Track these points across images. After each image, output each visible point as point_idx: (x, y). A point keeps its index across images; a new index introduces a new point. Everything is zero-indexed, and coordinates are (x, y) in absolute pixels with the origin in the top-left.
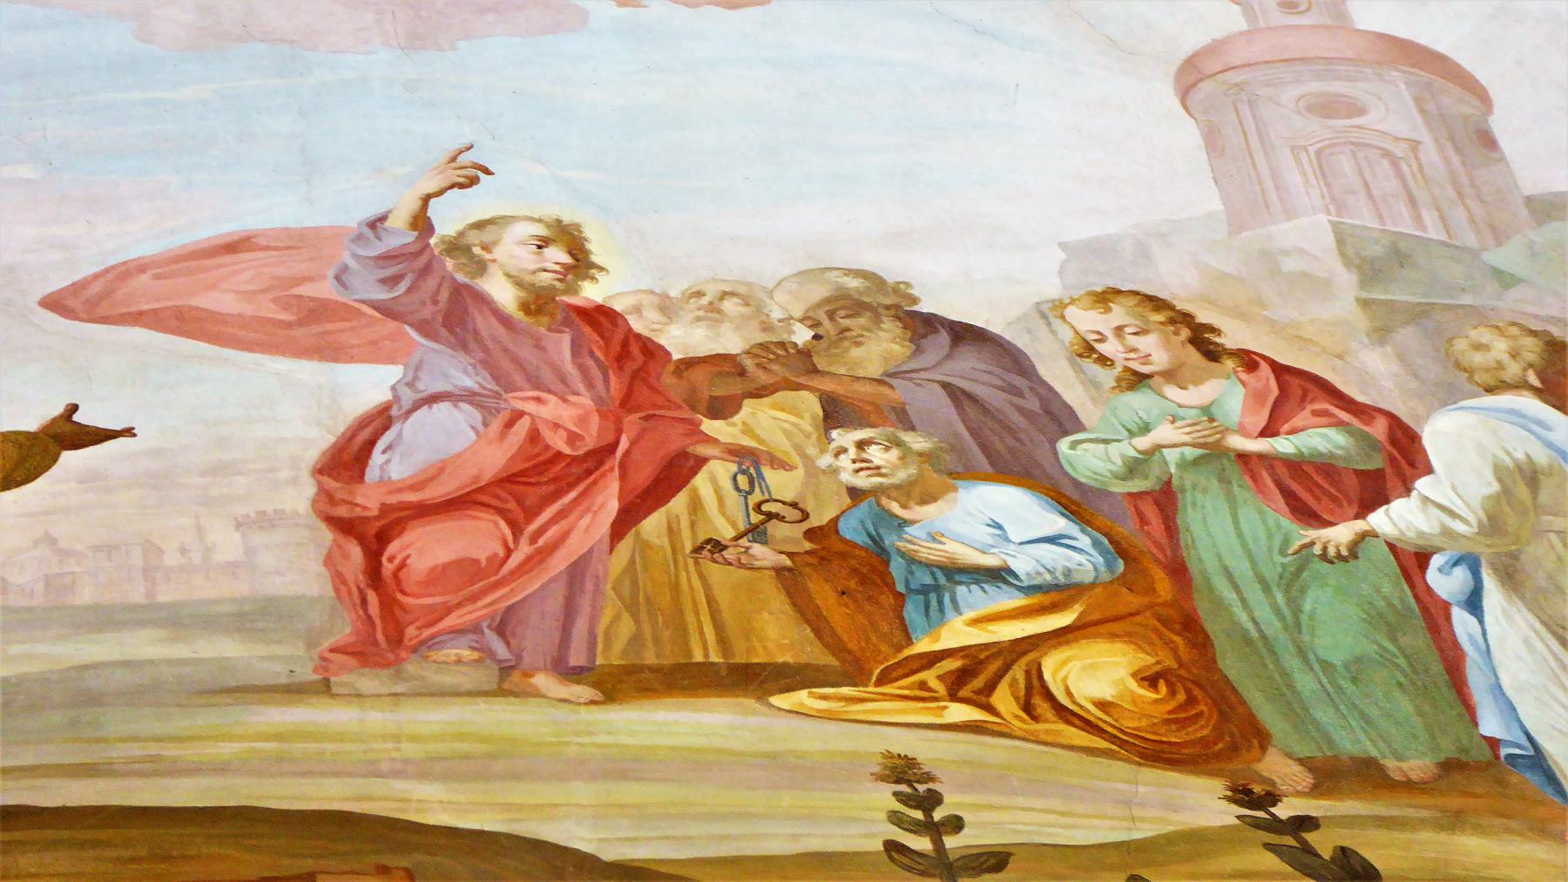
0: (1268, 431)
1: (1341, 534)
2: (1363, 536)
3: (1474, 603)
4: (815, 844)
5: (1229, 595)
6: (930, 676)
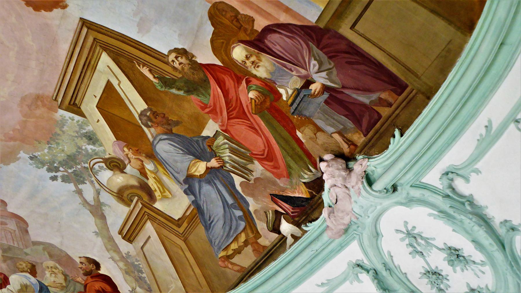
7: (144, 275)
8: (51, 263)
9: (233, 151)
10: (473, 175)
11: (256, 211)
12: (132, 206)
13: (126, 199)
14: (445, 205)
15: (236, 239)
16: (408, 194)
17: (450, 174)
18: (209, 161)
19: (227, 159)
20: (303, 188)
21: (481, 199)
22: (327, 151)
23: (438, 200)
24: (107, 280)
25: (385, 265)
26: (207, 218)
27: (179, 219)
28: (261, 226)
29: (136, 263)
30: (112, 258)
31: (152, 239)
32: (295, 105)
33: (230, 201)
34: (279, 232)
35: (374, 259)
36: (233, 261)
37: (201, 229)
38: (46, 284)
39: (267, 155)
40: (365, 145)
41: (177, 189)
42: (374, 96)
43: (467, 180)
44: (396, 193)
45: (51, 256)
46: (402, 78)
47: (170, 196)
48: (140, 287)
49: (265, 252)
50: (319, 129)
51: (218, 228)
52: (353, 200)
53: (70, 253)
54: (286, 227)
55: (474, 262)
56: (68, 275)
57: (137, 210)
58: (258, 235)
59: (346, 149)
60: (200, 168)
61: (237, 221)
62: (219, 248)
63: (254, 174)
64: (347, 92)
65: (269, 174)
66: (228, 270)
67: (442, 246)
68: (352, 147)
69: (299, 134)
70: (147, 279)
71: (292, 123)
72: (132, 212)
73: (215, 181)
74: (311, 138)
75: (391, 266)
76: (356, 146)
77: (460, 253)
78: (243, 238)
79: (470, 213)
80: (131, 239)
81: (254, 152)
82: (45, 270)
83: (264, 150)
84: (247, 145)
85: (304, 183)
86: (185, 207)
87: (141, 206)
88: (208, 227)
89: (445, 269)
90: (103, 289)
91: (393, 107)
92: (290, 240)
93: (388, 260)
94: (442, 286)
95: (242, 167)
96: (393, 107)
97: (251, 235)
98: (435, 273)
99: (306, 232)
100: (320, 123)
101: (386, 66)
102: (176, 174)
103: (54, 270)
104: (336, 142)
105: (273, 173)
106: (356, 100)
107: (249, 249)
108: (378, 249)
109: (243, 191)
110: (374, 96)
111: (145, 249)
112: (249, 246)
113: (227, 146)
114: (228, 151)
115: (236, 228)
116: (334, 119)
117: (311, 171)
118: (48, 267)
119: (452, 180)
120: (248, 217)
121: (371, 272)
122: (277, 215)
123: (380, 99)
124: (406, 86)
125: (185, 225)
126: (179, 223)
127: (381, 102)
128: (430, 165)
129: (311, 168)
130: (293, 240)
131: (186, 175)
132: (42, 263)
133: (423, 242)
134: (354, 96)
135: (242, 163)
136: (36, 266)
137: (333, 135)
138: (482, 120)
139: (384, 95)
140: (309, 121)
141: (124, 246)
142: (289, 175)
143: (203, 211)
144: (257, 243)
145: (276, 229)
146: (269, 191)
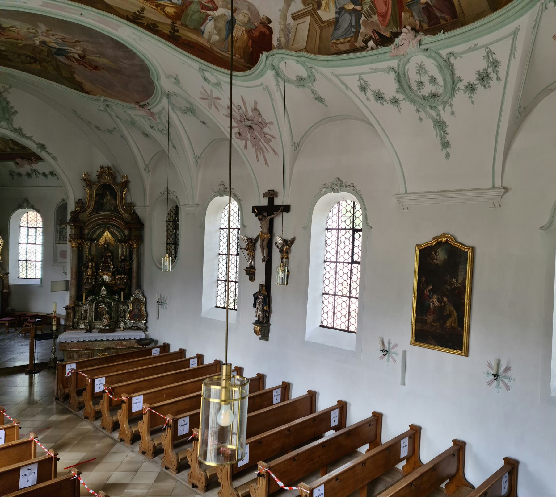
0: (206, 3)
1: (204, 11)
2: (205, 12)
3: (210, 20)
4: (127, 9)
5: (189, 11)
6: (154, 4)
7: (290, 34)
8: (247, 12)
9: (370, 7)
10: (459, 58)
11: (362, 32)
12: (307, 7)
13: (306, 3)
14: (443, 64)
15: (345, 38)
16: (431, 53)
17: (451, 54)
18: (357, 6)
19: (365, 9)
20: (389, 33)
21: (455, 67)
22: (409, 25)
23: (440, 61)
24: (270, 30)
25: (404, 73)
26: (338, 25)
27: (325, 21)
28: (360, 38)
29: (290, 29)
30: (280, 23)
31: (306, 23)
32: (410, 3)
33: (354, 24)
34: (366, 44)
35: (400, 69)
36: (338, 46)
37: (332, 29)
38: (236, 19)
39: (384, 15)
40: (427, 30)
41: (333, 9)
42: (443, 15)
43: (456, 58)
44: (427, 52)
45: (249, 9)
46: (458, 14)
47: (328, 11)
48: (284, 38)
49: (355, 48)
50: (412, 16)
51: (340, 32)
52: (409, 48)
53: (260, 12)
54: (371, 43)
55: (439, 85)
56: (251, 20)
57: (308, 9)
58: (356, 41)
59: (418, 27)
60: (351, 7)
61: (351, 32)
62: (334, 39)
63: (372, 19)
64: (434, 8)
65: (378, 22)
66: (332, 48)
67: (430, 75)
68: (421, 28)
69: (403, 14)
70: (290, 37)
71: (403, 9)
72: (304, 9)
73: (353, 15)
74: (407, 18)
75: (406, 74)
76: (422, 28)
77: (436, 80)
78: (349, 39)
79: (450, 70)
80: (296, 19)
81: (379, 12)
82: (241, 13)
83: (383, 13)
84: (377, 7)
85: (391, 32)
86: (331, 17)
87: (311, 8)
88: (335, 29)
89: (426, 82)
90: (264, 32)
91: (447, 22)
92: (370, 48)
93: (406, 71)
94: (421, 88)
95: (369, 14)
96: (447, 22)
97: (353, 40)
98: (421, 83)
99: (379, 48)
100: (414, 14)
101: (456, 7)
102: (337, 4)
103: (246, 15)
104: (416, 24)
105: (380, 22)
106: (435, 13)
107: (348, 44)
108: (405, 66)
109: (362, 23)
110: (443, 15)
111: (299, 25)
112: (349, 43)
113: (369, 4)
114: (368, 6)
115: (349, 35)
116: (421, 15)
117: (397, 29)
118: (243, 13)
119: (450, 56)
120: (357, 34)
121: (397, 73)
122: (371, 38)
123: (445, 17)
124: (458, 17)
125: (326, 24)
126: (323, 22)
127: (444, 18)
128: (446, 47)
129: (398, 28)
130: (370, 49)
131: (342, 6)
132: (241, 10)
133: (424, 71)
134: (436, 11)
135: (370, 13)
136: (237, 10)
137: (417, 21)
138: (475, 42)
139: (447, 17)
140: (411, 11)
141: (290, 20)
142: (387, 26)
143: (338, 23)
144: (354, 44)
145: (366, 42)
146: (374, 28)
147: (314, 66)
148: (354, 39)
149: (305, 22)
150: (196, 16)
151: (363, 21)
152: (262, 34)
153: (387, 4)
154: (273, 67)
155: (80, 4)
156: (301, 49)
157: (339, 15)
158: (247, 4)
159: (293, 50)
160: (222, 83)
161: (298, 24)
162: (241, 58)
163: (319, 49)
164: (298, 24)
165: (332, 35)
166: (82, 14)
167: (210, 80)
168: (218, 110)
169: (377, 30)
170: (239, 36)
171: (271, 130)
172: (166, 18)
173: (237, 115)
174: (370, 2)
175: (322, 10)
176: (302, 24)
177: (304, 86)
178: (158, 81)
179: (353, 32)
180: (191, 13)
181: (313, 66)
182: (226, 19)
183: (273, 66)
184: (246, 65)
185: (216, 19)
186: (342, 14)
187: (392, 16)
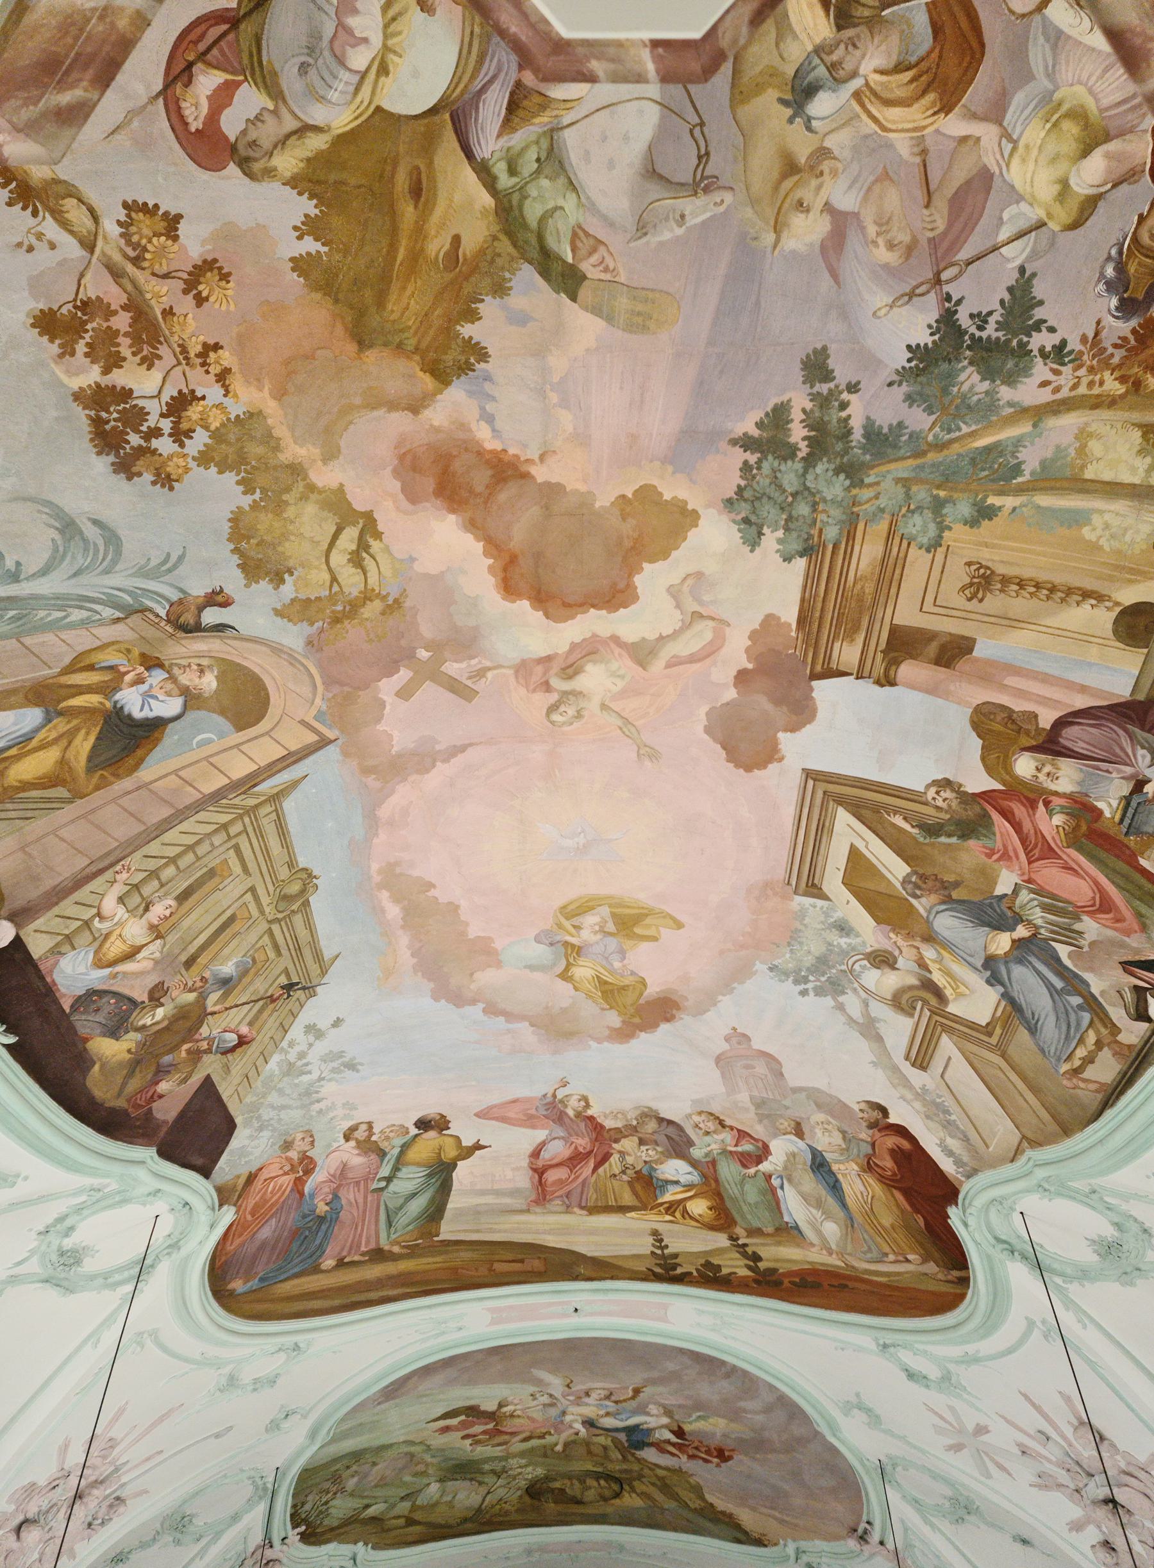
3: (782, 1187)
6: (661, 1208)
7: (953, 1117)
9: (1046, 908)
11: (1102, 993)
19: (1039, 922)
24: (901, 1131)
26: (1029, 1015)
28: (1117, 1014)
30: (902, 1097)
31: (953, 1060)
32: (1127, 822)
33: (1059, 984)
37: (1023, 1034)
41: (976, 981)
45: (819, 1106)
47: (968, 992)
49: (1134, 1054)
51: (1050, 1030)
58: (1115, 1030)
62: (1059, 1059)
65: (1110, 933)
66: (1079, 1091)
69: (1143, 862)
71: (1129, 848)
78: (1091, 1038)
83: (1094, 898)
84: (1064, 895)
87: (928, 1014)
88: (1033, 1030)
95: (1065, 929)
97: (1104, 1032)
102: (968, 959)
105: (1115, 929)
109: (1076, 966)
111: (946, 1077)
112: (1106, 1049)
114: (1038, 909)
115: (1078, 1024)
126: (988, 1030)
141: (916, 1077)
144: (1117, 1042)
147: (1097, 1182)
148: (1106, 1027)
149: (950, 1058)
150: (752, 1194)
151: (1070, 956)
152: (896, 1154)
153: (1076, 867)
154: (1006, 1246)
155: (555, 1284)
156: (1016, 1144)
157: (1003, 985)
158: (804, 1094)
159: (994, 1163)
160: (952, 1367)
161: (942, 1076)
162: (925, 1261)
163: (1053, 1117)
164: (942, 1076)
165: (1042, 1051)
166: (576, 1310)
167: (924, 1372)
168: (1010, 1474)
169: (1130, 958)
170: (865, 1194)
171: (230, 1428)
172: (705, 1232)
173: (1055, 1469)
174: (1032, 896)
175: (955, 999)
176: (949, 1069)
177: (1139, 1270)
178: (838, 1434)
179: (1080, 1007)
180: (736, 1191)
181: (1093, 1181)
182: (805, 1163)
183: (1005, 1242)
184: (950, 1277)
185: (787, 1175)
186: (1005, 977)
187: (1124, 889)
